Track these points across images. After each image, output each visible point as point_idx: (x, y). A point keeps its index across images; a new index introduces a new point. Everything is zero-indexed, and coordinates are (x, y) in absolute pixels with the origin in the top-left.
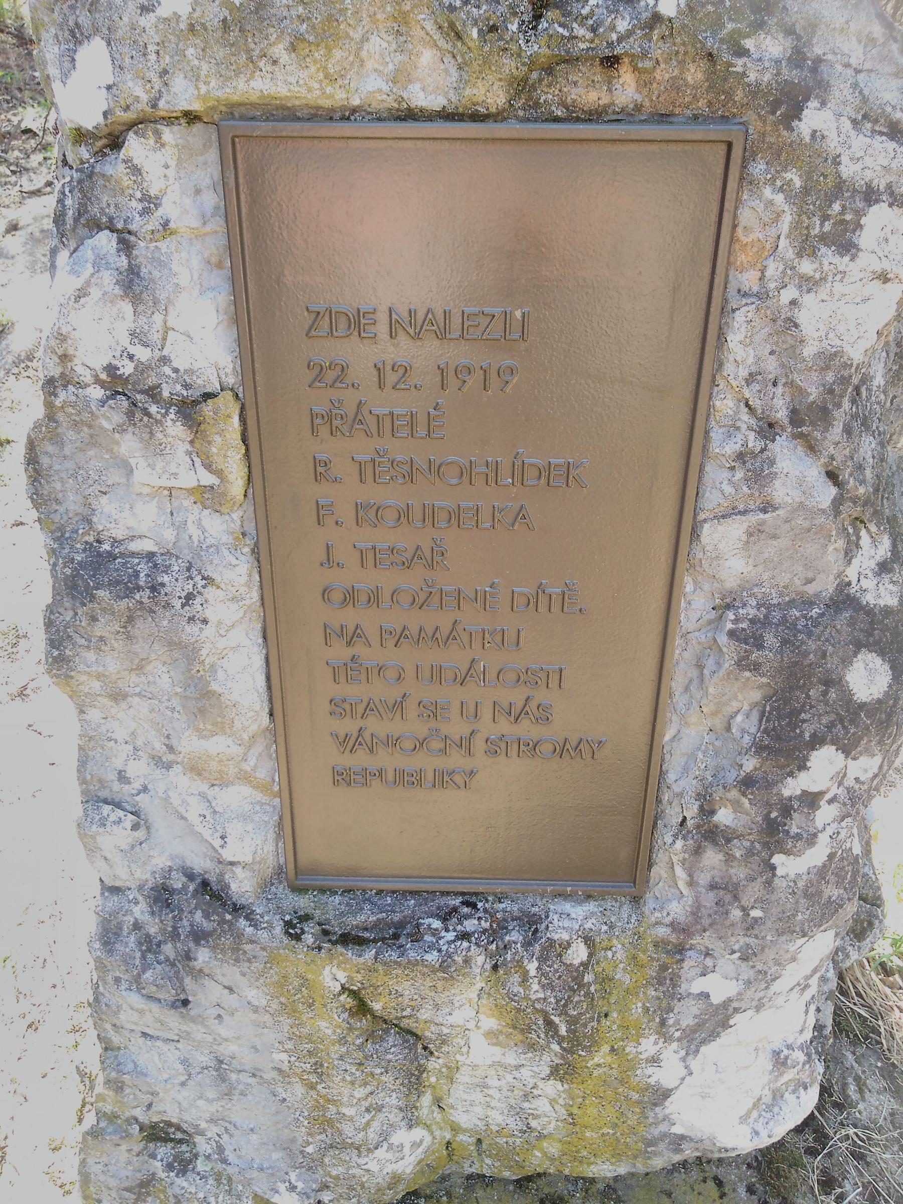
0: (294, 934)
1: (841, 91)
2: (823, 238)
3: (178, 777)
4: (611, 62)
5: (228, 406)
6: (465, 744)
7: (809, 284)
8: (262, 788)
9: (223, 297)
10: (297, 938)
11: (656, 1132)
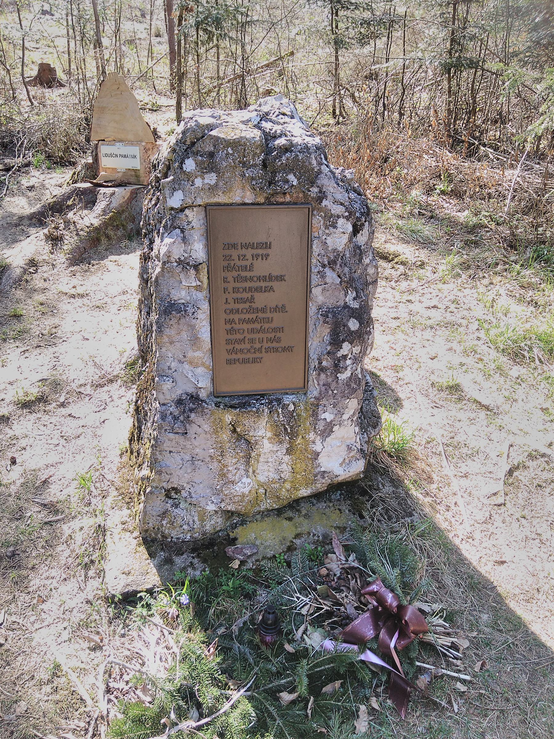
0: (217, 405)
1: (330, 197)
2: (330, 225)
3: (186, 366)
4: (285, 194)
5: (205, 266)
6: (260, 350)
7: (328, 235)
8: (207, 368)
9: (204, 242)
10: (219, 407)
11: (317, 470)
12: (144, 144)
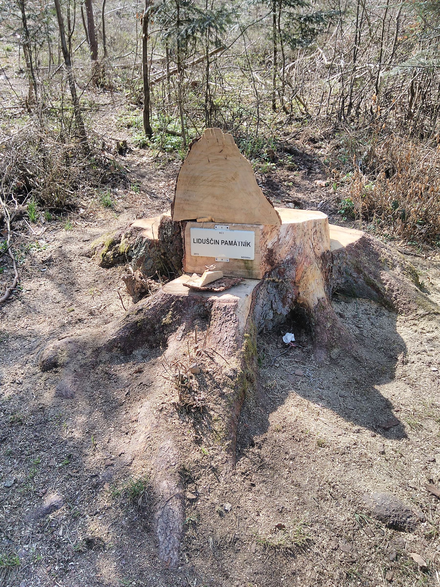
12: (262, 227)
